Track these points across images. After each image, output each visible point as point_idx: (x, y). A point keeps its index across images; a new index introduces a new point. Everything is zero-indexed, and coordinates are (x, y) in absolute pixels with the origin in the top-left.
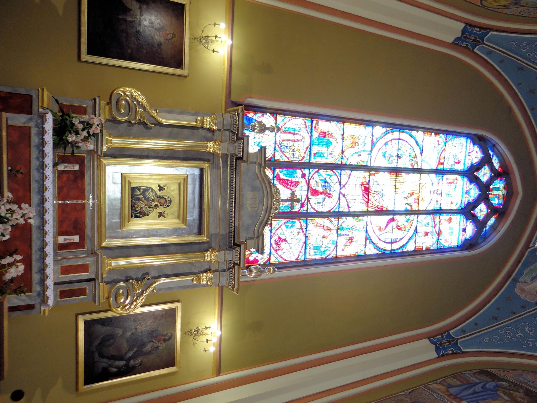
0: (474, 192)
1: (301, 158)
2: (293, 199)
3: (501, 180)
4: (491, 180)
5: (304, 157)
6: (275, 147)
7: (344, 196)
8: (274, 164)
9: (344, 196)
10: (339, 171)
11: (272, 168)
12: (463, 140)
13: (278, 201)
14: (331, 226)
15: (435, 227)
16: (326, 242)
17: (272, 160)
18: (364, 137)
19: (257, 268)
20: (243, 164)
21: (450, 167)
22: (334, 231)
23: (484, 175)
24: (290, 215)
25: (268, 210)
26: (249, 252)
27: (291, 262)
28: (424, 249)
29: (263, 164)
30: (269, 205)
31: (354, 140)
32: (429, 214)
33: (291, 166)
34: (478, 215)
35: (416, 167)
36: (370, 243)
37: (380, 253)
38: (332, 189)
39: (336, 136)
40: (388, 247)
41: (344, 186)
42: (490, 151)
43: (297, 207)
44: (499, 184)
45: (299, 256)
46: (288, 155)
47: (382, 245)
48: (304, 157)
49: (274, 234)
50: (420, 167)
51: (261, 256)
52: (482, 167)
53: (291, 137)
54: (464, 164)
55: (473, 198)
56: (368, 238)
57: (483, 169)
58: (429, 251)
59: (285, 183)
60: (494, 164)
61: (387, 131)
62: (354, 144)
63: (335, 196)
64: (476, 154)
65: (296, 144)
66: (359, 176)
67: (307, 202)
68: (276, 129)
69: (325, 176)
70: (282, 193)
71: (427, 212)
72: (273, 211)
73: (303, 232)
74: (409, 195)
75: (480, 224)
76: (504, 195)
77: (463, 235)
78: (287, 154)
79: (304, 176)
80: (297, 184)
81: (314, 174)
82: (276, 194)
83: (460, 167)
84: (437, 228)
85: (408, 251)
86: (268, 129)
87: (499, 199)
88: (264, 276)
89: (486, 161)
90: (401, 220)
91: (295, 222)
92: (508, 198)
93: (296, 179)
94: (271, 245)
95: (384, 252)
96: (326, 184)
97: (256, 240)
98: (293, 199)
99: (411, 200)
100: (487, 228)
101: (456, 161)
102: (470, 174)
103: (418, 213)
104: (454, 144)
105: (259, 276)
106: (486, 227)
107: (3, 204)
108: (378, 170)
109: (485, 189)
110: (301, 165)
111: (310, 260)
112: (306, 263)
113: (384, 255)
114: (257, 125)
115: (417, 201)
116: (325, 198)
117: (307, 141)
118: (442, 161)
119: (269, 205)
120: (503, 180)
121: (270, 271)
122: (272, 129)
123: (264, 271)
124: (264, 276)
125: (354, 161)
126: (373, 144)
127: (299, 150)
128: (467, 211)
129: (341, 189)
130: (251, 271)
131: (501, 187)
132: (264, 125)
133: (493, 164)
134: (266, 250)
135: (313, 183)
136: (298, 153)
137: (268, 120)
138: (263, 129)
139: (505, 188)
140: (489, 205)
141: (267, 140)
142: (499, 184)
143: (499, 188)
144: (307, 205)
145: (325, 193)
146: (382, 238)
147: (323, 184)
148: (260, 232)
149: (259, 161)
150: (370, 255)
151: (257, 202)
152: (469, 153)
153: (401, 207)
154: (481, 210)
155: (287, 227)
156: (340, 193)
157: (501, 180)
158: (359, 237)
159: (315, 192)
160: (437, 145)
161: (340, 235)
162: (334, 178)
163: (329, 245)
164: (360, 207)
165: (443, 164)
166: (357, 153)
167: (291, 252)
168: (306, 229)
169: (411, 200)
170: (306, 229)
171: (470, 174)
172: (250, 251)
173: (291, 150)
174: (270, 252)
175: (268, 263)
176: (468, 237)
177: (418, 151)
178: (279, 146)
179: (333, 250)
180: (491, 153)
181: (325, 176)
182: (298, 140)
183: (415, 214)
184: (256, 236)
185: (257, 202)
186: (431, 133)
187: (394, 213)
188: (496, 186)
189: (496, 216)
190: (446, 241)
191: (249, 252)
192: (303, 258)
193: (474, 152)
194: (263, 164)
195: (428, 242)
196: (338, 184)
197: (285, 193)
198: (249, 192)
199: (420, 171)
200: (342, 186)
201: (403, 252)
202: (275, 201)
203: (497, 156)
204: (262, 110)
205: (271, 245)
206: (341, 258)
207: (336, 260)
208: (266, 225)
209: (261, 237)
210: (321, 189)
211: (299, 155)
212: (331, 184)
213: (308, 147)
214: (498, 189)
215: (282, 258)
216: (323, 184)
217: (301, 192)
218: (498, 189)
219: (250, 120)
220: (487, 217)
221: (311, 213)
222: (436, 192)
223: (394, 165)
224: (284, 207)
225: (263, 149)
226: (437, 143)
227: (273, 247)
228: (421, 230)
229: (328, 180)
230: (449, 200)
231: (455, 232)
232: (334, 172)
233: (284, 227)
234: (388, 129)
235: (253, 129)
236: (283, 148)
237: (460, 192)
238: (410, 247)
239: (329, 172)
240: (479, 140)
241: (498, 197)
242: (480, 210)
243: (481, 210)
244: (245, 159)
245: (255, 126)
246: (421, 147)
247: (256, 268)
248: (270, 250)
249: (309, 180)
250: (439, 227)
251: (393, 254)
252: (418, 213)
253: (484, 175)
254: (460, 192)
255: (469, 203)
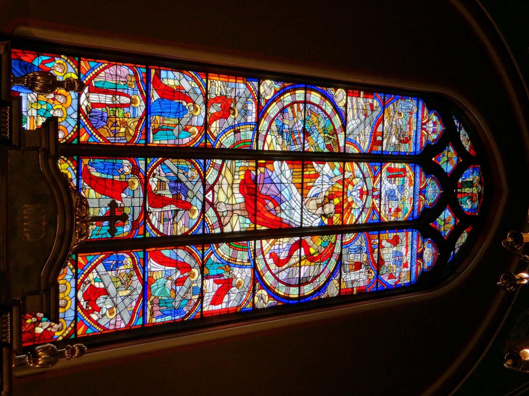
0: (433, 191)
1: (129, 139)
2: (115, 216)
3: (474, 169)
4: (459, 170)
5: (135, 136)
6: (79, 118)
7: (212, 205)
8: (76, 150)
9: (212, 205)
10: (202, 161)
11: (75, 158)
12: (411, 104)
13: (88, 220)
14: (188, 260)
15: (373, 251)
16: (182, 290)
17: (75, 142)
18: (243, 100)
19: (47, 348)
20: (12, 152)
21: (392, 149)
22: (196, 271)
23: (447, 161)
24: (111, 246)
25: (66, 238)
26: (34, 320)
27: (117, 332)
28: (355, 292)
29: (52, 152)
30: (67, 228)
31: (210, 102)
32: (362, 231)
33: (111, 152)
34: (442, 229)
35: (336, 150)
36: (261, 288)
37: (280, 304)
38: (189, 193)
39: (193, 96)
40: (294, 292)
41: (212, 188)
42: (455, 121)
43: (124, 230)
44: (471, 176)
45: (131, 320)
46: (104, 132)
47: (282, 290)
48: (135, 136)
49: (82, 281)
50: (342, 151)
51: (56, 326)
52: (445, 149)
53: (107, 99)
54: (416, 144)
55: (431, 201)
56: (257, 278)
57: (446, 152)
58: (363, 294)
59: (98, 185)
60: (464, 143)
61: (285, 87)
62: (226, 111)
63: (197, 205)
64: (433, 127)
65: (120, 113)
66: (235, 171)
67: (145, 219)
68: (74, 86)
69: (175, 170)
70: (91, 203)
71: (356, 228)
72: (76, 238)
73: (138, 274)
74: (327, 200)
75: (443, 244)
76: (480, 193)
77: (418, 264)
78: (103, 132)
79: (135, 170)
80: (124, 186)
81: (155, 167)
82: (80, 207)
83: (407, 148)
84: (375, 255)
85: (328, 298)
86: (61, 84)
87: (473, 201)
88: (62, 363)
89: (449, 137)
90: (316, 244)
91: (124, 257)
92: (487, 199)
93: (123, 176)
94: (77, 302)
95: (286, 301)
96: (179, 185)
97: (44, 296)
98: (115, 216)
99: (329, 208)
100: (456, 251)
101: (402, 139)
102: (424, 160)
103: (342, 230)
104: (398, 108)
105: (53, 363)
106: (454, 249)
107: (336, 176)
108: (271, 156)
109: (449, 184)
110: (130, 151)
111: (155, 326)
112: (147, 332)
113: (285, 306)
114: (39, 78)
115: (341, 209)
116: (177, 211)
117: (140, 107)
118: (379, 138)
119: (67, 228)
120: (478, 170)
121: (73, 351)
122: (69, 85)
123: (63, 353)
124: (62, 363)
125: (228, 141)
126: (261, 113)
127: (124, 124)
128: (421, 223)
129: (205, 193)
130: (35, 357)
131: (475, 181)
132: (54, 77)
133: (460, 142)
134: (67, 313)
135: (153, 183)
136: (126, 127)
137: (62, 69)
138: (51, 84)
139: (480, 182)
140: (457, 211)
141: (64, 108)
142: (471, 176)
143: (471, 182)
144: (145, 224)
145: (176, 201)
146: (283, 276)
147: (173, 185)
148: (50, 281)
149: (44, 146)
150: (263, 309)
151: (44, 224)
152: (423, 124)
153: (313, 221)
154: (446, 220)
155: (108, 268)
156: (205, 200)
157: (474, 169)
158: (242, 276)
159: (159, 201)
160: (369, 113)
161: (208, 277)
162: (193, 173)
163: (189, 296)
164: (239, 223)
165: (381, 143)
166: (233, 127)
167: (115, 313)
168: (144, 268)
169: (329, 208)
170: (144, 268)
171: (424, 160)
172: (35, 316)
173: (110, 124)
174: (76, 316)
175: (73, 336)
176: (426, 266)
177: (337, 122)
178: (85, 117)
179: (196, 304)
180: (457, 124)
181: (175, 170)
182: (122, 106)
183: (337, 233)
184: (43, 287)
185: (44, 224)
186: (360, 91)
187: (302, 231)
188: (468, 180)
189: (469, 229)
190: (391, 276)
191: (34, 320)
192: (140, 322)
193: (431, 124)
194: (52, 152)
195: (358, 279)
196: (200, 184)
197: (97, 203)
198: (26, 206)
199: (344, 157)
200: (207, 187)
201: (320, 299)
202: (78, 220)
203: (466, 130)
204: (54, 50)
205: (77, 302)
206: (210, 318)
207: (205, 321)
208: (63, 265)
209: (52, 290)
210: (168, 194)
211: (126, 133)
212: (188, 184)
213: (141, 118)
214: (470, 184)
215: (99, 325)
216: (173, 185)
217: (131, 201)
218: (470, 184)
219: (28, 67)
220: (456, 232)
221: (151, 238)
222: (370, 192)
223: (297, 148)
224: (97, 232)
225: (52, 123)
226: (369, 107)
227: (81, 307)
228: (352, 258)
229: (183, 178)
230: (394, 205)
231: (402, 259)
232: (193, 164)
233: (101, 267)
234: (286, 84)
235: (31, 88)
236: (94, 121)
237: (401, 193)
238: (333, 291)
239: (184, 163)
240: (433, 103)
241: (471, 198)
242: (444, 220)
243: (446, 220)
244: (15, 141)
245: (34, 79)
246: (344, 115)
247: (44, 350)
248: (76, 311)
249: (147, 178)
250: (379, 253)
251: (302, 304)
252: (342, 230)
253: (448, 161)
254: (401, 193)
255: (425, 208)
